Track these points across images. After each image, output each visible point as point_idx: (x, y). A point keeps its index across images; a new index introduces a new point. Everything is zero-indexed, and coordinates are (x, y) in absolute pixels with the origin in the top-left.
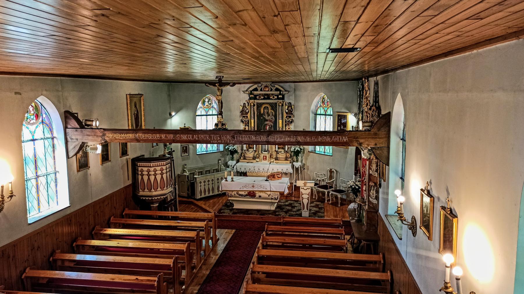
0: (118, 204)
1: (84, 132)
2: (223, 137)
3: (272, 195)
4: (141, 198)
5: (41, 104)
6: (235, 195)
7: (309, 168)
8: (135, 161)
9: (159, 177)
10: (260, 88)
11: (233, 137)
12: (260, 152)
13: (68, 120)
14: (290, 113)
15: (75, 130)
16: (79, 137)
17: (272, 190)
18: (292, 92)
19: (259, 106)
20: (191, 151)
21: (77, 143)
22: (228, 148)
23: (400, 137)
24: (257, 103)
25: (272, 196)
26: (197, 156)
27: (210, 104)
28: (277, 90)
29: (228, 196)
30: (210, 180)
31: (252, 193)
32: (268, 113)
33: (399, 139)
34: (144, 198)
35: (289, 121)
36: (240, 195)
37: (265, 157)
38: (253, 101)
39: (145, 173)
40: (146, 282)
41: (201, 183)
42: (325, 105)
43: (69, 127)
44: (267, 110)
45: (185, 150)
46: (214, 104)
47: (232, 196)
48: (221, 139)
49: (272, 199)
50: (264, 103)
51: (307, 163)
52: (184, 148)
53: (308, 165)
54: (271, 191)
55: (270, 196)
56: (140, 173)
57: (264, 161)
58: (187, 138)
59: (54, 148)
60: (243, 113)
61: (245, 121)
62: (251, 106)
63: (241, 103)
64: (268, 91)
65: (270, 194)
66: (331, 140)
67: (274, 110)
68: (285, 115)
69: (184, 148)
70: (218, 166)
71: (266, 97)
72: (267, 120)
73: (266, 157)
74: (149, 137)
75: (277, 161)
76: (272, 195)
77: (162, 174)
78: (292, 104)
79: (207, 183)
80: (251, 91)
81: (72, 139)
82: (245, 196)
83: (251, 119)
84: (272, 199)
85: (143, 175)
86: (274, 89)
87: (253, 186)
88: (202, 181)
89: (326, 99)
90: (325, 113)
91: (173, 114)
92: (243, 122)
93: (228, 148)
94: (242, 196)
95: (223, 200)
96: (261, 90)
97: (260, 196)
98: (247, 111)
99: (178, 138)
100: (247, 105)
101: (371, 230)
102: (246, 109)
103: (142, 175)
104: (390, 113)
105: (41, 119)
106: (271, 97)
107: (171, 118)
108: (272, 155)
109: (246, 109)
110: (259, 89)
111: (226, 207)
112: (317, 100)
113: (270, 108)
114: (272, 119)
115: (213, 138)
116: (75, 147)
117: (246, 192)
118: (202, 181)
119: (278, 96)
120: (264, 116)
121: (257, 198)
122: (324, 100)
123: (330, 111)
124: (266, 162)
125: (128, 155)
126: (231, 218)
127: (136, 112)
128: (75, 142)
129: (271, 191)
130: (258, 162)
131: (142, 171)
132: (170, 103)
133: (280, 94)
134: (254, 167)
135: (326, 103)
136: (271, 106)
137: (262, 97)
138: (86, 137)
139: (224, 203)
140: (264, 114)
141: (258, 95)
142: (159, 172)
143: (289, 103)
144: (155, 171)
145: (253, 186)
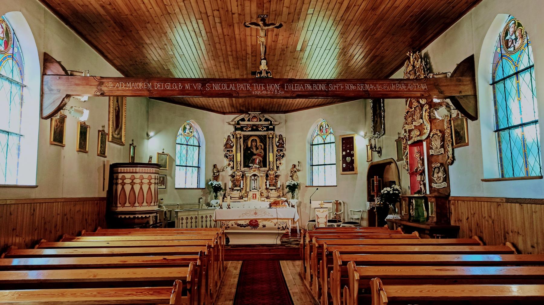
0: (90, 216)
1: (70, 80)
2: (269, 86)
3: (279, 223)
4: (119, 217)
5: (14, 33)
6: (232, 225)
8: (114, 167)
9: (145, 188)
10: (248, 118)
11: (282, 87)
12: (248, 190)
13: (48, 64)
14: (281, 146)
15: (57, 77)
16: (62, 88)
17: (279, 217)
18: (282, 124)
19: (246, 138)
20: (169, 184)
21: (59, 95)
22: (212, 184)
23: (488, 82)
24: (244, 136)
25: (280, 225)
26: (176, 191)
27: (191, 132)
28: (267, 120)
30: (194, 217)
31: (255, 222)
32: (256, 146)
33: (488, 85)
34: (123, 216)
35: (280, 155)
36: (239, 225)
37: (254, 196)
38: (240, 132)
39: (128, 181)
40: (181, 261)
41: (182, 219)
42: (323, 133)
43: (48, 74)
44: (255, 143)
45: (162, 181)
46: (195, 133)
48: (266, 89)
49: (279, 228)
50: (251, 136)
52: (162, 178)
53: (305, 202)
54: (277, 219)
55: (277, 225)
56: (120, 181)
58: (221, 88)
59: (22, 100)
60: (228, 146)
61: (229, 155)
62: (237, 138)
64: (257, 121)
66: (406, 88)
68: (275, 149)
69: (162, 178)
70: (198, 205)
71: (254, 127)
72: (255, 155)
73: (255, 194)
74: (167, 87)
76: (279, 223)
77: (150, 184)
78: (283, 137)
79: (189, 221)
80: (238, 121)
81: (51, 90)
82: (245, 227)
83: (237, 153)
85: (125, 183)
86: (263, 119)
87: (256, 213)
88: (184, 218)
89: (324, 126)
90: (324, 141)
91: (151, 134)
92: (227, 157)
93: (212, 184)
94: (241, 227)
96: (249, 120)
97: (264, 226)
98: (232, 144)
99: (208, 89)
100: (232, 137)
101: (443, 222)
102: (231, 142)
103: (123, 184)
104: (473, 56)
105: (11, 51)
106: (260, 129)
107: (148, 139)
108: (262, 193)
109: (231, 142)
110: (246, 119)
112: (314, 129)
113: (258, 141)
114: (261, 153)
115: (256, 88)
116: (54, 102)
118: (184, 218)
119: (267, 127)
120: (252, 150)
121: (260, 229)
122: (322, 127)
123: (331, 138)
124: (256, 201)
125: (105, 157)
127: (117, 108)
128: (55, 94)
129: (277, 219)
130: (246, 201)
131: (124, 178)
132: (148, 119)
133: (271, 124)
135: (324, 131)
136: (259, 138)
137: (250, 129)
138: (73, 87)
140: (251, 147)
141: (245, 127)
142: (146, 181)
143: (280, 135)
144: (142, 178)
145: (256, 213)
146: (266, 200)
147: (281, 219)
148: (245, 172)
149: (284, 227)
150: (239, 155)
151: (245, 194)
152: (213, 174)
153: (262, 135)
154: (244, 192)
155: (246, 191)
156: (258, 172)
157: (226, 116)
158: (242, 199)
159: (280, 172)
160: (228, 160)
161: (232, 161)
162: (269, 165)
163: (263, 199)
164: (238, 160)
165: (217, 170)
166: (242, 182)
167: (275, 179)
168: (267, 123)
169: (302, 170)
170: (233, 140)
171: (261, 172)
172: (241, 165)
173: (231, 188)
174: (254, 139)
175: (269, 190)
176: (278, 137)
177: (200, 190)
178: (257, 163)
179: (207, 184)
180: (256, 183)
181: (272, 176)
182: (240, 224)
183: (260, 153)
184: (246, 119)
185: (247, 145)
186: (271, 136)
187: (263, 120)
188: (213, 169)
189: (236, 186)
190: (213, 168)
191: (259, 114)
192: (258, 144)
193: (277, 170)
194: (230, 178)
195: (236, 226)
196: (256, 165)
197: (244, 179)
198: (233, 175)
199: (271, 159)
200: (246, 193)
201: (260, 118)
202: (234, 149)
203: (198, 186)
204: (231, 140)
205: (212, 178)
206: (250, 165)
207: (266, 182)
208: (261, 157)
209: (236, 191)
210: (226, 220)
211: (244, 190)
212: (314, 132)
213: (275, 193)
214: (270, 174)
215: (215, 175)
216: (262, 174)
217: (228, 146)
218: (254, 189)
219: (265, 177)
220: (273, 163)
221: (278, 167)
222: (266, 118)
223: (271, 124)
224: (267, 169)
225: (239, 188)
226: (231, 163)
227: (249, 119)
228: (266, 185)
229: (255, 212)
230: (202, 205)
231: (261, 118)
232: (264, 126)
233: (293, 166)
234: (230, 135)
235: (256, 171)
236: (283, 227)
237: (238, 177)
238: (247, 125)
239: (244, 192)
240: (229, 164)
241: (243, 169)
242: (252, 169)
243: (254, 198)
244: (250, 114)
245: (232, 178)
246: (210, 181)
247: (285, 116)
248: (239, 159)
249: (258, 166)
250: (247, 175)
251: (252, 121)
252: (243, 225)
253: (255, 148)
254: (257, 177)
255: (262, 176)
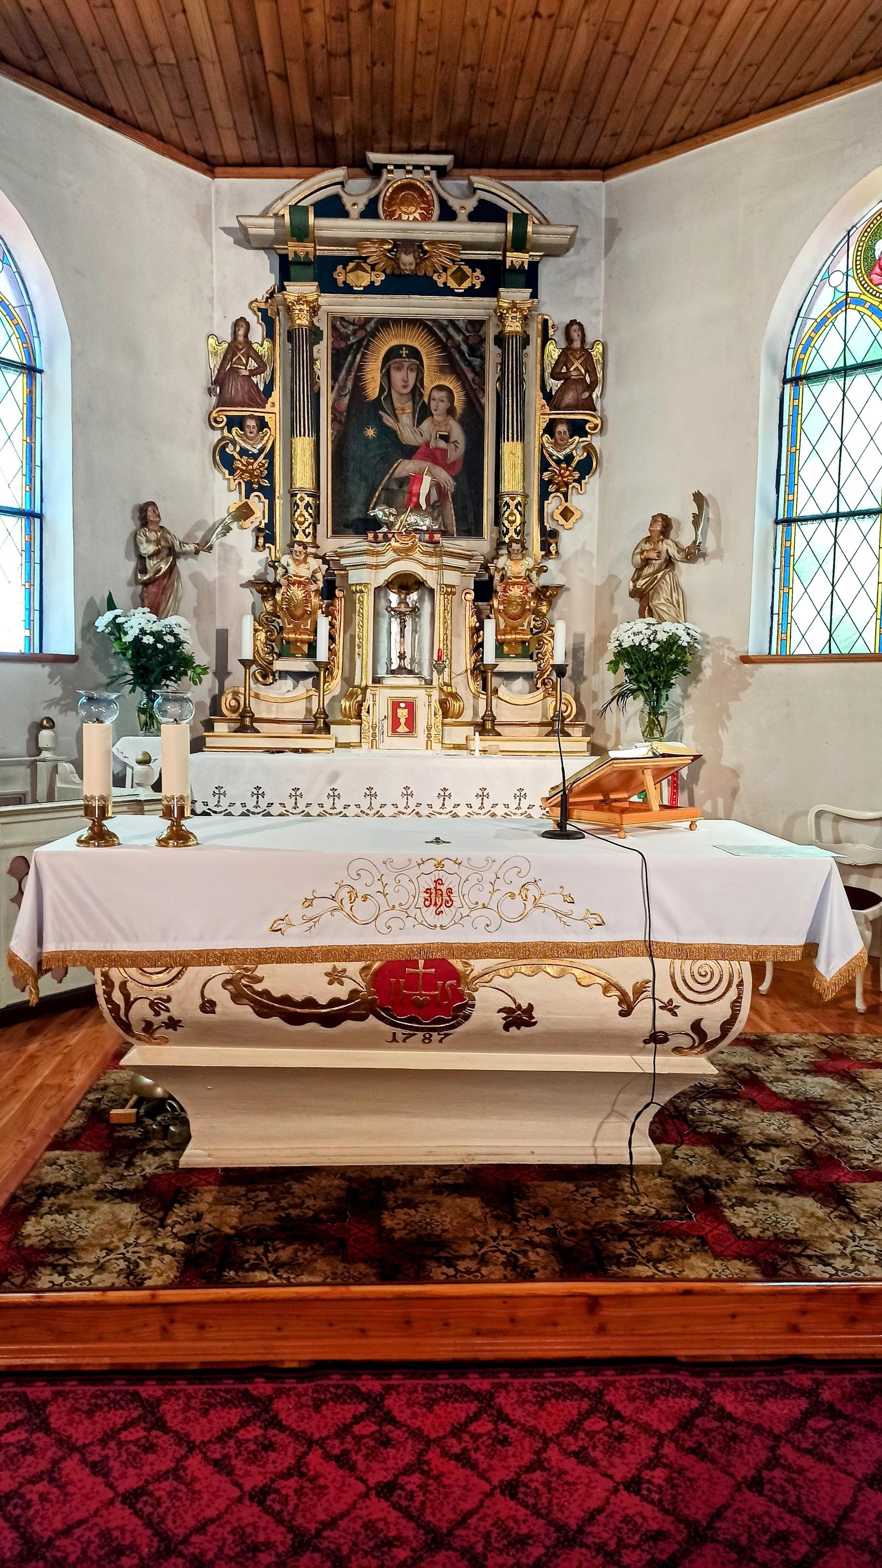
3: (665, 992)
6: (208, 1006)
7: (744, 782)
10: (363, 202)
12: (362, 677)
17: (662, 934)
22: (117, 628)
24: (338, 322)
25: (670, 1008)
29: (126, 1026)
31: (429, 982)
32: (416, 392)
35: (569, 458)
37: (403, 713)
44: (412, 376)
47: (173, 1024)
49: (657, 1038)
50: (385, 323)
51: (727, 749)
53: (728, 760)
54: (650, 949)
55: (644, 1006)
57: (398, 742)
61: (243, 452)
63: (217, 316)
64: (425, 218)
65: (639, 990)
67: (460, 377)
72: (410, 452)
73: (411, 706)
75: (491, 742)
78: (590, 339)
82: (330, 1021)
84: (657, 1038)
93: (117, 628)
95: (65, 1069)
96: (370, 212)
98: (259, 381)
102: (253, 364)
109: (253, 364)
110: (355, 203)
111: (90, 1156)
113: (430, 359)
114: (446, 438)
117: (353, 968)
120: (389, 421)
126: (165, 1333)
129: (650, 949)
130: (347, 745)
133: (519, 242)
134: (335, 776)
139: (71, 1098)
146: (478, 742)
147: (683, 952)
148: (344, 561)
149: (712, 1029)
150: (303, 445)
151: (345, 704)
152: (132, 564)
153: (452, 322)
154: (335, 686)
155: (348, 680)
156: (424, 559)
157: (225, 184)
158: (327, 729)
159: (562, 571)
160: (234, 484)
161: (261, 489)
162: (497, 521)
163: (458, 734)
164: (298, 484)
165: (158, 542)
166: (323, 624)
167: (536, 612)
168: (489, 232)
169: (719, 553)
170: (263, 348)
171: (447, 560)
172: (317, 517)
173: (253, 662)
174: (400, 347)
175: (495, 682)
176: (558, 336)
177: (42, 671)
178: (422, 501)
179: (87, 629)
180: (414, 631)
181: (516, 591)
182: (286, 1000)
183: (442, 444)
184: (355, 203)
185: (359, 388)
186: (513, 326)
187: (463, 214)
188: (135, 535)
189: (286, 650)
190: (131, 525)
191: (442, 172)
192: (430, 381)
193: (548, 554)
194: (249, 597)
195: (246, 1012)
196: (412, 519)
197: (339, 604)
198: (271, 579)
199: (511, 483)
200: (350, 696)
201: (443, 202)
202: (276, 409)
203: (29, 639)
204: (250, 352)
205: (123, 594)
206: (379, 513)
207: (478, 630)
208: (448, 468)
209: (289, 682)
210: (140, 960)
211: (338, 673)
212: (823, 275)
213: (529, 698)
214: (503, 577)
215: (144, 571)
216: (451, 578)
217: (235, 389)
218: (401, 670)
219: (471, 597)
220: (523, 507)
221: (554, 534)
222: (482, 202)
223: (519, 242)
224: (482, 546)
225: (302, 665)
226: (258, 504)
227: (373, 202)
228: (478, 648)
229: (428, 882)
230: (55, 769)
231: (454, 203)
232: (468, 262)
233: (658, 527)
234: (253, 319)
235: (417, 555)
236: (696, 1026)
237: (298, 593)
238: (357, 243)
239: (337, 692)
240: (244, 513)
241: (330, 545)
242: (386, 539)
243: (403, 729)
244: (376, 171)
245: (264, 599)
246: (111, 606)
247: (610, 193)
248: (303, 478)
249: (425, 523)
250: (354, 577)
251: (390, 216)
252: (310, 1002)
253: (409, 407)
254: (421, 599)
255: (450, 591)
